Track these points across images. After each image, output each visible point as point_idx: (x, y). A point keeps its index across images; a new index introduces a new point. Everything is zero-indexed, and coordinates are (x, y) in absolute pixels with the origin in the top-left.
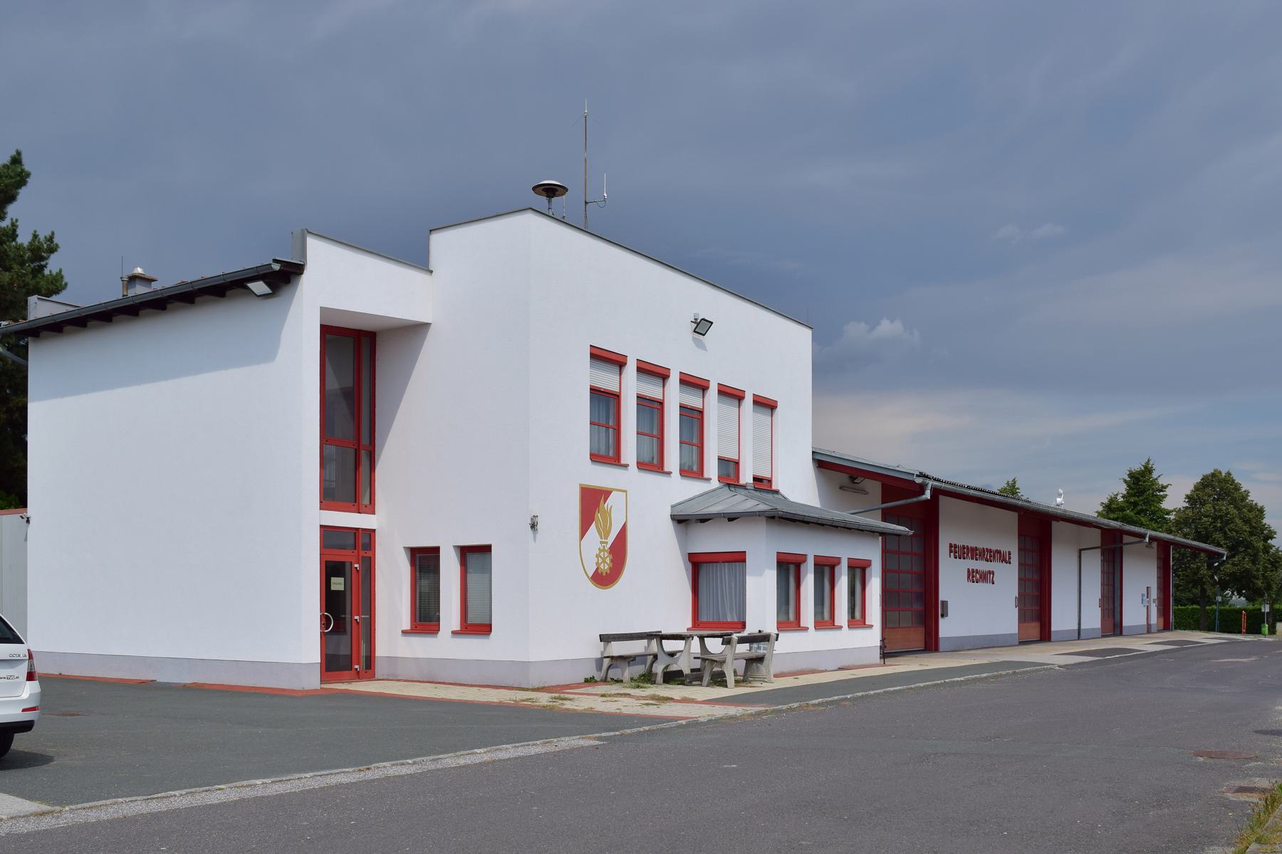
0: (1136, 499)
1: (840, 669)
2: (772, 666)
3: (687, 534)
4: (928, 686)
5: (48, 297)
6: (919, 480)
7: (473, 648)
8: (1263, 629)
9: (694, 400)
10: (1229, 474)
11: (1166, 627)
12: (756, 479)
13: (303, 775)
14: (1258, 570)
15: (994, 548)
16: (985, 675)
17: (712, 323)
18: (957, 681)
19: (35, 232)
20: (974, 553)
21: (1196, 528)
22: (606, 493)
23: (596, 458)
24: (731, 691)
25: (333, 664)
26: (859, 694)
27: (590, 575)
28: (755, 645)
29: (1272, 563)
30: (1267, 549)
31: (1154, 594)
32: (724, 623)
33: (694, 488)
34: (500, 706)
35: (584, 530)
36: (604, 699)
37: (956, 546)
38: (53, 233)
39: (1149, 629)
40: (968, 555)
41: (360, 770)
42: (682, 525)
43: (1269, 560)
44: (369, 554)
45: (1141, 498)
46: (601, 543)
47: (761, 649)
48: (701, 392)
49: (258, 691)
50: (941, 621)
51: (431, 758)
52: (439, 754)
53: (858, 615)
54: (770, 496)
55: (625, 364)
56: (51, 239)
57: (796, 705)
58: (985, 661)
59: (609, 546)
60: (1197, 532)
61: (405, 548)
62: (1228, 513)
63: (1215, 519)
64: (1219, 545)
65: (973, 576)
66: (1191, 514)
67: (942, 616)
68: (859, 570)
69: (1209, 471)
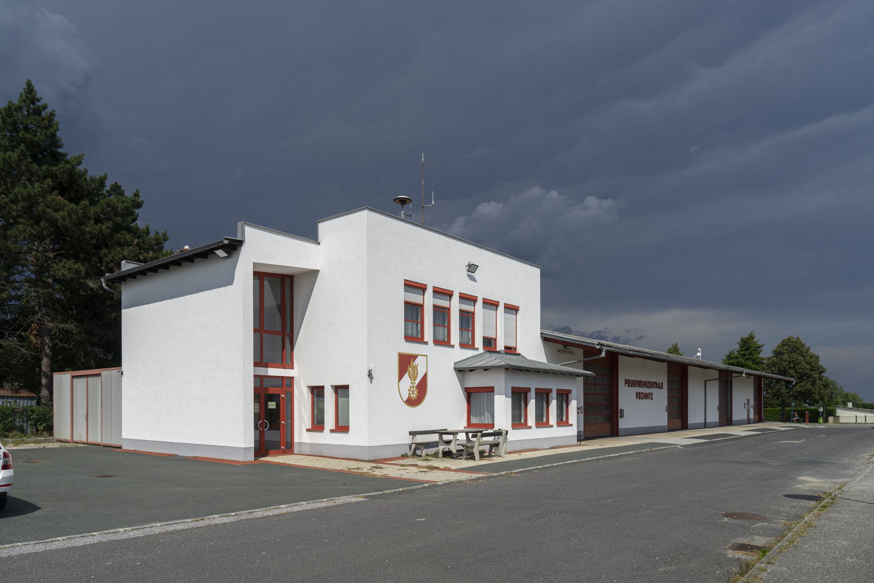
0: (745, 352)
1: (552, 448)
2: (502, 449)
3: (464, 378)
4: (593, 460)
6: (598, 347)
7: (340, 439)
8: (819, 421)
9: (468, 308)
10: (798, 338)
11: (760, 420)
12: (506, 348)
13: (153, 525)
14: (816, 389)
15: (652, 381)
16: (632, 452)
17: (478, 266)
18: (613, 456)
19: (29, 84)
20: (640, 384)
21: (778, 367)
22: (415, 357)
23: (408, 338)
24: (478, 462)
25: (262, 448)
26: (547, 466)
27: (405, 400)
28: (497, 437)
29: (824, 386)
30: (820, 379)
31: (752, 403)
32: (484, 424)
33: (469, 353)
34: (340, 473)
35: (401, 377)
36: (402, 468)
37: (629, 380)
38: (166, 231)
39: (749, 422)
40: (636, 384)
41: (196, 521)
42: (461, 373)
43: (822, 384)
44: (290, 389)
45: (748, 352)
46: (411, 383)
47: (500, 439)
48: (473, 303)
49: (220, 462)
50: (620, 420)
51: (248, 511)
52: (255, 509)
53: (564, 419)
54: (515, 357)
55: (426, 289)
56: (165, 235)
57: (504, 473)
58: (639, 442)
59: (416, 385)
60: (779, 369)
61: (331, 386)
62: (797, 359)
63: (789, 362)
64: (792, 376)
65: (639, 396)
66: (775, 360)
67: (621, 417)
68: (564, 397)
69: (786, 337)
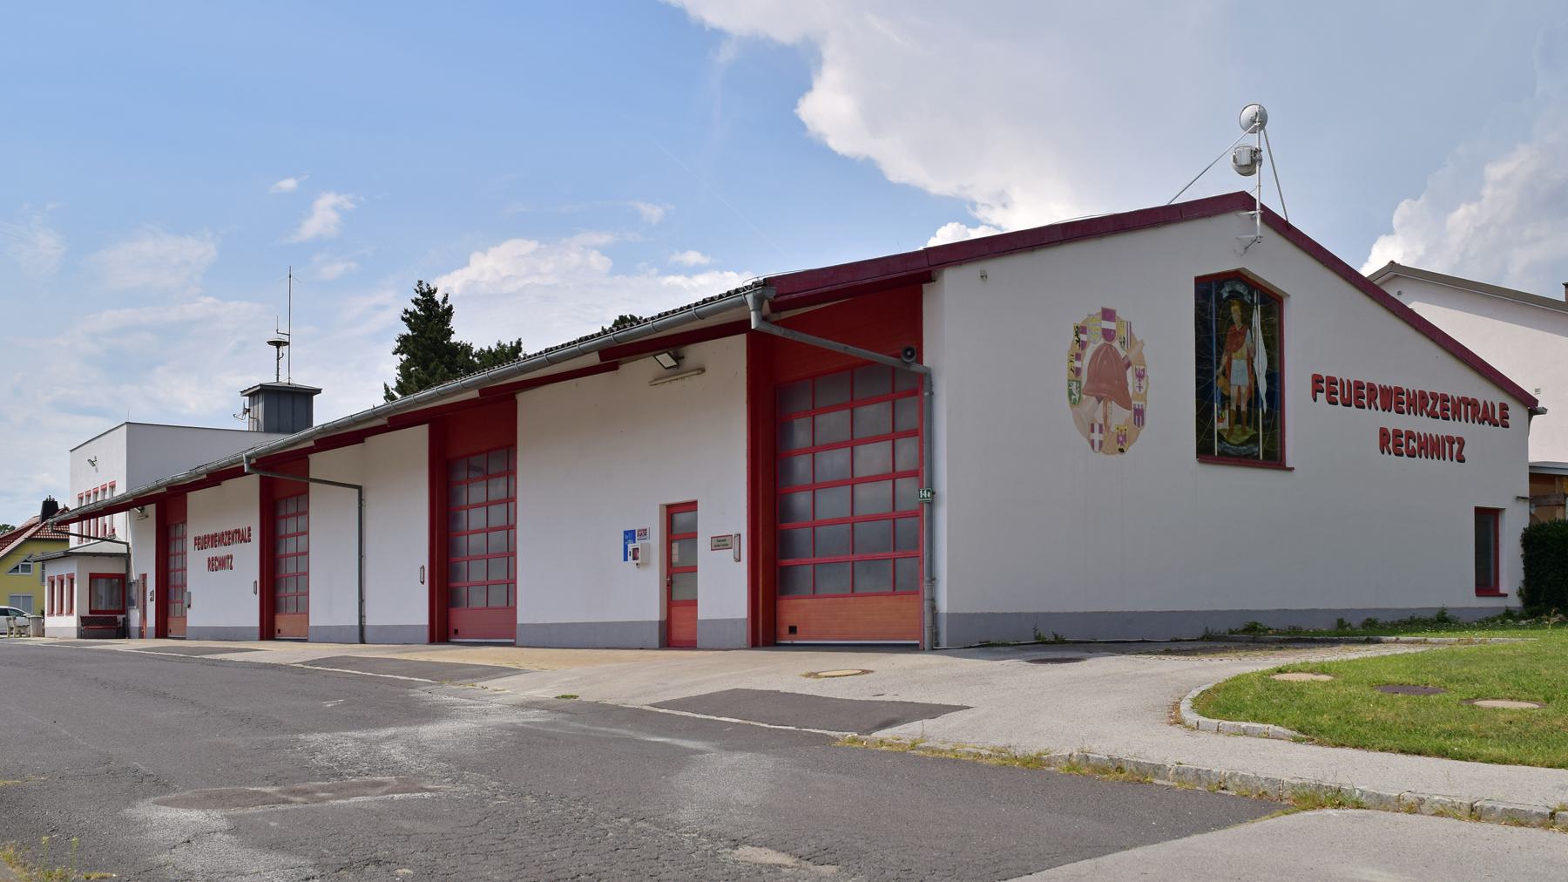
1: (1172, 641)
4: (779, 733)
5: (1255, 200)
15: (232, 529)
19: (520, 339)
37: (1332, 381)
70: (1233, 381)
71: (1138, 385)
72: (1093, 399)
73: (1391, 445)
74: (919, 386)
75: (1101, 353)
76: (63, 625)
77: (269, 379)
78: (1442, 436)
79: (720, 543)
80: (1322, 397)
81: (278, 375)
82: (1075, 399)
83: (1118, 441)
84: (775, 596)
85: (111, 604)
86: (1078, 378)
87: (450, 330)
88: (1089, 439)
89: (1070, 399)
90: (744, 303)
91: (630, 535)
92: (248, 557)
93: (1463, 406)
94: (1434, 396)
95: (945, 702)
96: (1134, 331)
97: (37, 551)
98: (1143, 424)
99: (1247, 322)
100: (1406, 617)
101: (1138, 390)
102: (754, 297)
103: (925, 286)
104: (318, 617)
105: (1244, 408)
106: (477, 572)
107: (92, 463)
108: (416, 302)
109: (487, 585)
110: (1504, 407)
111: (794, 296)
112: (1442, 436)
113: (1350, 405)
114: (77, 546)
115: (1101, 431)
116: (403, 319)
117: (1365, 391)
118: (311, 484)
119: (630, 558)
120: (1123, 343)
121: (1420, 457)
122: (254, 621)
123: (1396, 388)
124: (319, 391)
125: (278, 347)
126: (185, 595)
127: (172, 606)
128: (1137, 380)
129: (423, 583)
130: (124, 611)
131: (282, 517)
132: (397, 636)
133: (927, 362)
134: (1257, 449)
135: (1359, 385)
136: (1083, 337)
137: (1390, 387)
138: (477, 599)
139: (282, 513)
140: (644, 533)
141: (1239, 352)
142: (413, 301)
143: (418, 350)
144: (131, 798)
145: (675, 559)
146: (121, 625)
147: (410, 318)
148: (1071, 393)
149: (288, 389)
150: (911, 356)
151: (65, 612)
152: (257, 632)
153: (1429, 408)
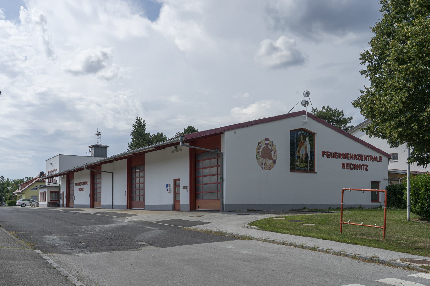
15: (84, 181)
19: (162, 132)
70: (301, 153)
71: (274, 155)
72: (263, 158)
73: (345, 167)
74: (220, 156)
75: (265, 148)
76: (43, 204)
77: (96, 144)
78: (361, 165)
79: (184, 188)
80: (325, 156)
81: (98, 142)
82: (258, 158)
83: (269, 167)
84: (195, 199)
85: (56, 199)
86: (259, 154)
87: (145, 129)
88: (261, 167)
89: (257, 158)
90: (179, 140)
91: (167, 186)
92: (87, 188)
93: (367, 157)
94: (359, 155)
95: (207, 222)
96: (273, 143)
97: (38, 185)
98: (276, 163)
99: (305, 140)
100: (349, 207)
101: (274, 156)
102: (181, 139)
103: (222, 135)
104: (103, 203)
105: (304, 159)
106: (137, 193)
107: (51, 164)
108: (136, 122)
109: (139, 196)
110: (380, 157)
111: (189, 139)
112: (361, 165)
113: (333, 158)
114: (47, 184)
115: (264, 165)
116: (133, 126)
117: (338, 155)
118: (102, 172)
119: (167, 191)
120: (270, 146)
121: (354, 169)
122: (89, 204)
123: (347, 154)
124: (108, 147)
125: (98, 136)
126: (73, 197)
127: (70, 200)
128: (274, 154)
129: (126, 195)
130: (59, 201)
131: (96, 179)
132: (120, 207)
133: (222, 152)
134: (307, 168)
135: (336, 153)
136: (260, 145)
137: (345, 153)
138: (137, 199)
139: (96, 178)
140: (170, 185)
141: (303, 147)
142: (135, 122)
143: (136, 135)
144: (45, 235)
145: (176, 191)
146: (58, 204)
147: (135, 126)
148: (257, 157)
149: (100, 146)
150: (217, 150)
151: (42, 201)
152: (90, 206)
153: (357, 158)
